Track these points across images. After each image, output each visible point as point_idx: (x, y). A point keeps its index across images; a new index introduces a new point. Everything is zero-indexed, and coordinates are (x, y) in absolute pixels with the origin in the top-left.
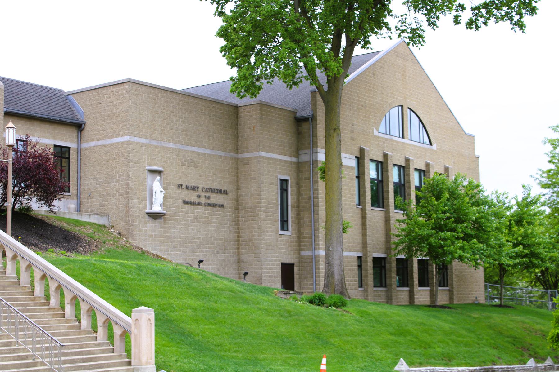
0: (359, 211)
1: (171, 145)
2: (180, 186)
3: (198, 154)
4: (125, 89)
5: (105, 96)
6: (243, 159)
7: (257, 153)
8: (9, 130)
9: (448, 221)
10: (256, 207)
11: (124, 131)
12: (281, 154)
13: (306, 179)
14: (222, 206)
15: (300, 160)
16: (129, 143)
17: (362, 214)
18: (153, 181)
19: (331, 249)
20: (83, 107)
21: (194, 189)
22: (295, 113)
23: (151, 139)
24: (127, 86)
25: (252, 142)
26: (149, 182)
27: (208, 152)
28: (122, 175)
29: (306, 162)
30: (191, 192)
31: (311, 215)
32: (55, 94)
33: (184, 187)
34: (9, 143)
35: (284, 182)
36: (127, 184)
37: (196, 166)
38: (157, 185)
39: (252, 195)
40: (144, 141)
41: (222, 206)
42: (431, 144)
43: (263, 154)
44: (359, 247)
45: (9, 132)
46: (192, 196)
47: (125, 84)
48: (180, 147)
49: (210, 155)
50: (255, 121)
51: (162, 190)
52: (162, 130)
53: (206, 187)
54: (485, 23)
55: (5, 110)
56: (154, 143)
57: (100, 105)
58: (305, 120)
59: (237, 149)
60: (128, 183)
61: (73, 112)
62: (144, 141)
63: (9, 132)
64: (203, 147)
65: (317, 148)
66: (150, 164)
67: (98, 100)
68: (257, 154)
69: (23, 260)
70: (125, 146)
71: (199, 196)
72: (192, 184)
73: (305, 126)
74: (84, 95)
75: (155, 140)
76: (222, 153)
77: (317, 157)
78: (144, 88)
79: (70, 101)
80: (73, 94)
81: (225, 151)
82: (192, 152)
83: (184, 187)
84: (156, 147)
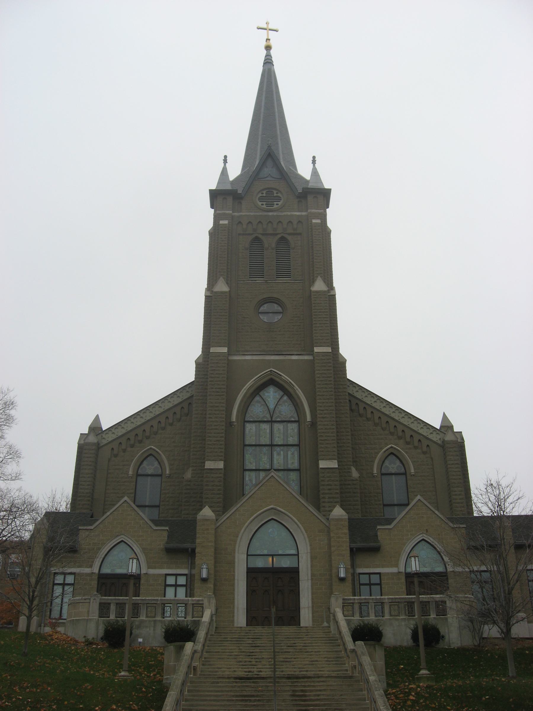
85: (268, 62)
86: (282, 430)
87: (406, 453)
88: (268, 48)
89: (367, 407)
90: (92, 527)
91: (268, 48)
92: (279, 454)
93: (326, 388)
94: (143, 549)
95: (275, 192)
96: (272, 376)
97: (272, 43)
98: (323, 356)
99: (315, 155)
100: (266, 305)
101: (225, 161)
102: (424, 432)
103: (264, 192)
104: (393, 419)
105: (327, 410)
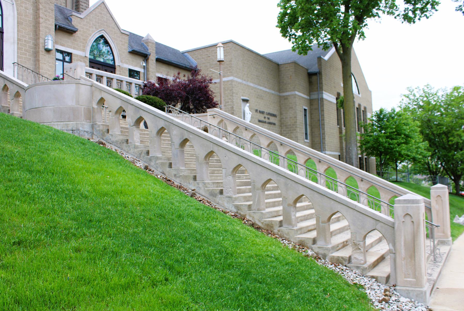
0: (338, 129)
1: (252, 85)
2: (256, 111)
3: (264, 91)
4: (229, 47)
5: (213, 52)
6: (284, 96)
7: (294, 92)
8: (220, 48)
9: (392, 134)
10: (293, 125)
11: (229, 74)
12: (304, 94)
13: (315, 109)
14: (274, 124)
15: (311, 98)
16: (232, 81)
17: (340, 131)
18: (245, 107)
19: (351, 149)
20: (195, 60)
21: (262, 113)
22: (307, 70)
23: (242, 79)
24: (230, 45)
25: (289, 85)
26: (242, 108)
27: (267, 90)
28: (228, 102)
29: (315, 99)
30: (261, 115)
31: (320, 130)
32: (177, 52)
33: (258, 111)
34: (220, 58)
35: (305, 110)
36: (233, 108)
37: (262, 99)
38: (247, 108)
39: (291, 118)
40: (239, 80)
41: (274, 124)
42: (359, 93)
43: (297, 93)
44: (339, 149)
45: (220, 50)
46: (261, 117)
47: (228, 44)
48: (256, 86)
49: (268, 93)
50: (291, 73)
51: (250, 112)
52: (247, 75)
53: (268, 112)
54: (419, 19)
55: (157, 57)
56: (244, 82)
57: (209, 58)
58: (315, 74)
59: (280, 90)
60: (233, 107)
61: (190, 63)
62: (239, 80)
63: (220, 50)
64: (266, 87)
65: (322, 90)
66: (243, 96)
67: (207, 55)
68: (293, 93)
69: (282, 147)
70: (229, 83)
71: (265, 118)
72: (262, 110)
73: (314, 78)
74: (196, 53)
75: (244, 80)
76: (273, 92)
77: (322, 96)
78: (238, 47)
79: (186, 56)
80: (188, 52)
81: (274, 90)
82: (261, 90)
83: (258, 111)
84: (245, 85)
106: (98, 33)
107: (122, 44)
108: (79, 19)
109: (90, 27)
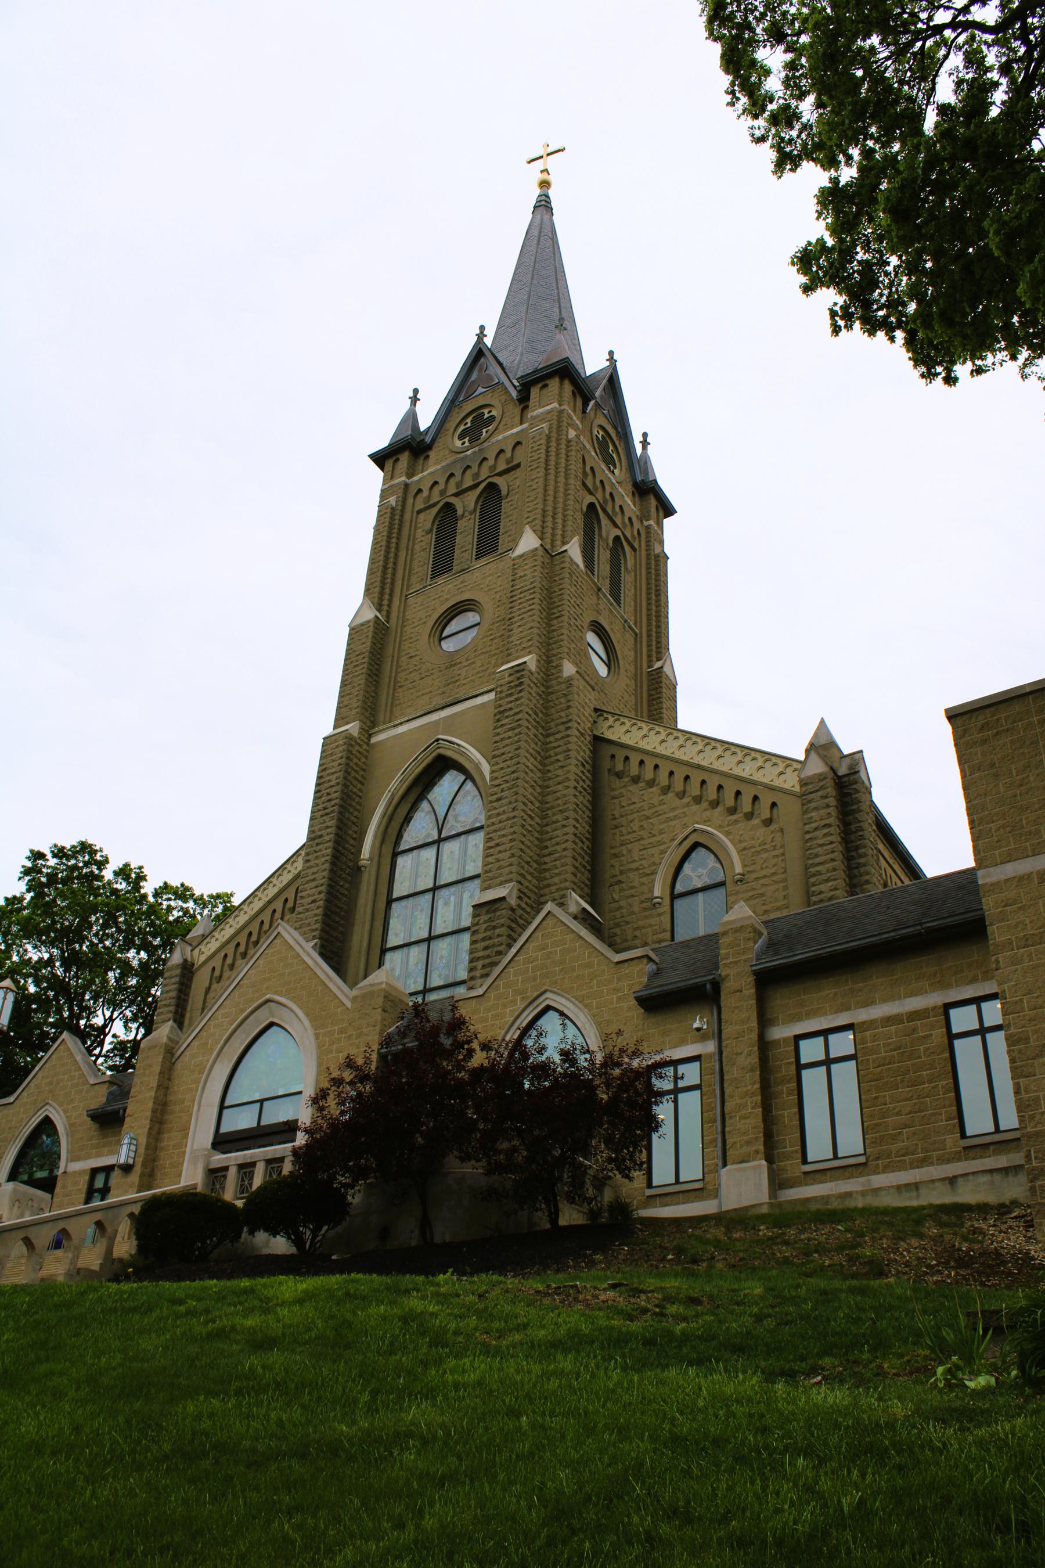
8: (6, 994)
85: (544, 205)
86: (457, 853)
87: (727, 834)
88: (545, 184)
89: (645, 758)
90: (11, 1099)
91: (545, 184)
92: (446, 904)
93: (509, 737)
94: (72, 1125)
95: (611, 448)
96: (439, 751)
97: (552, 178)
98: (511, 675)
99: (800, 291)
100: (453, 622)
101: (414, 399)
102: (768, 776)
103: (601, 433)
104: (699, 767)
105: (507, 781)
106: (531, 1008)
107: (619, 999)
108: (474, 1000)
109: (505, 1006)
